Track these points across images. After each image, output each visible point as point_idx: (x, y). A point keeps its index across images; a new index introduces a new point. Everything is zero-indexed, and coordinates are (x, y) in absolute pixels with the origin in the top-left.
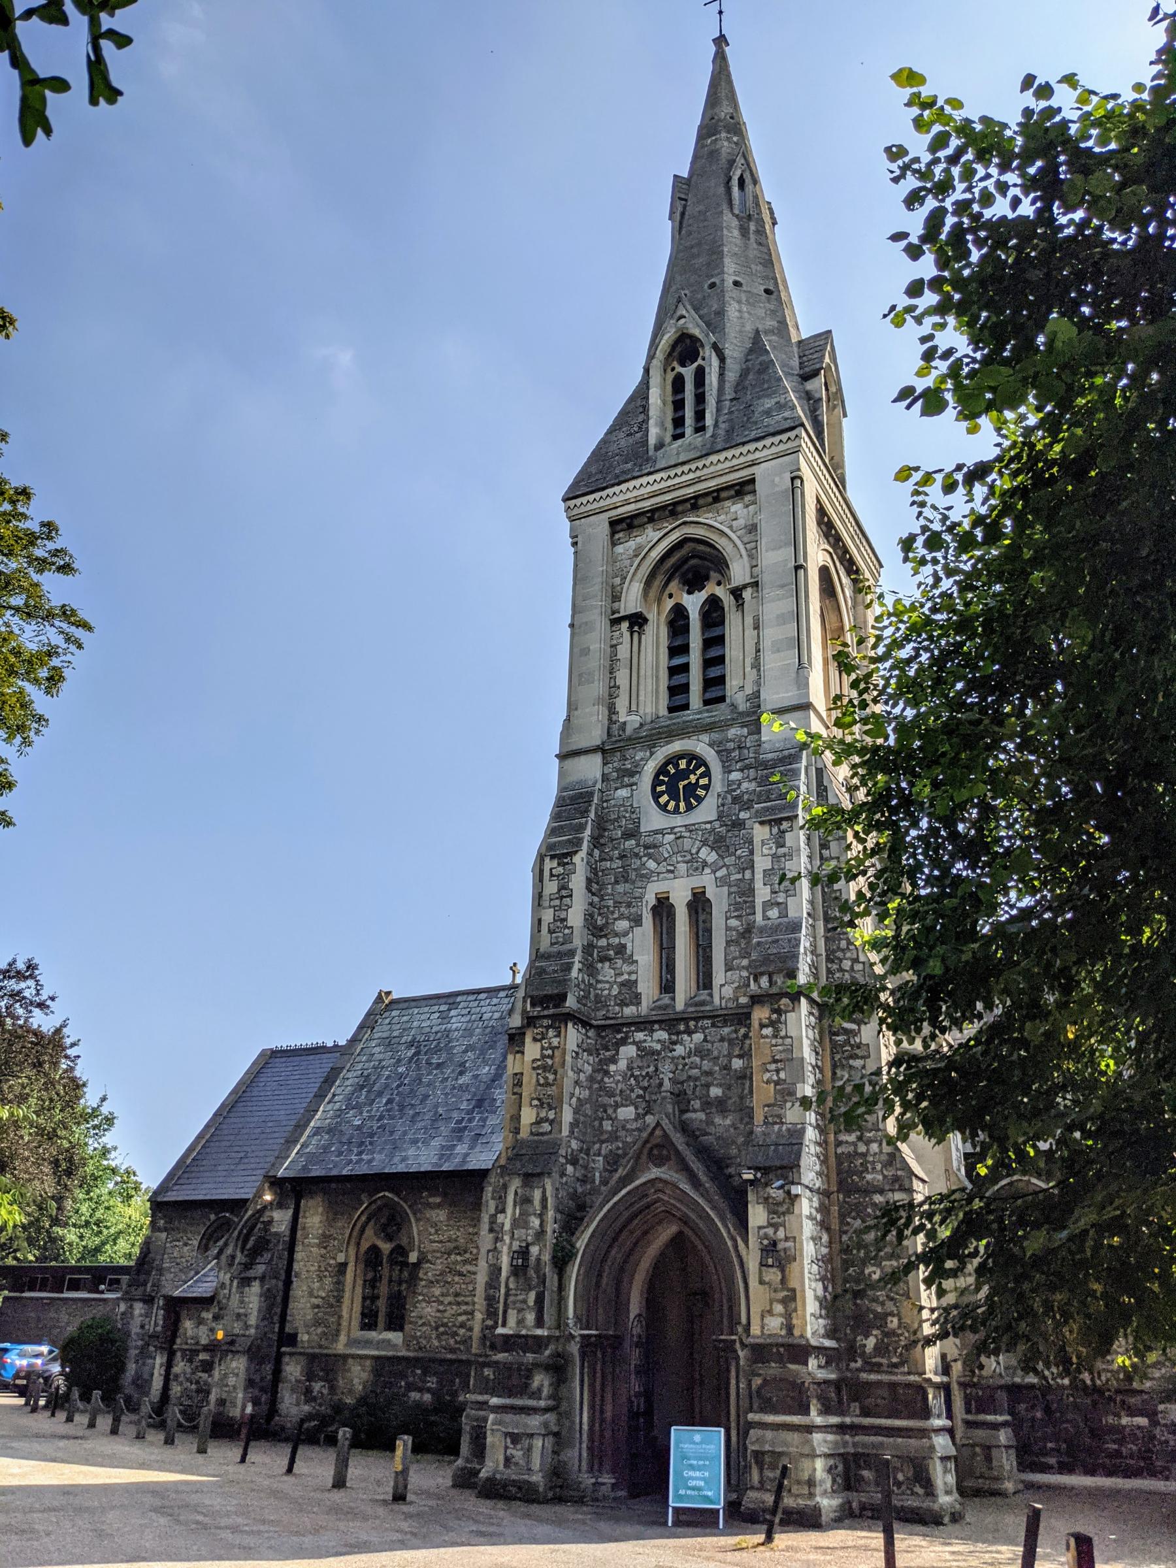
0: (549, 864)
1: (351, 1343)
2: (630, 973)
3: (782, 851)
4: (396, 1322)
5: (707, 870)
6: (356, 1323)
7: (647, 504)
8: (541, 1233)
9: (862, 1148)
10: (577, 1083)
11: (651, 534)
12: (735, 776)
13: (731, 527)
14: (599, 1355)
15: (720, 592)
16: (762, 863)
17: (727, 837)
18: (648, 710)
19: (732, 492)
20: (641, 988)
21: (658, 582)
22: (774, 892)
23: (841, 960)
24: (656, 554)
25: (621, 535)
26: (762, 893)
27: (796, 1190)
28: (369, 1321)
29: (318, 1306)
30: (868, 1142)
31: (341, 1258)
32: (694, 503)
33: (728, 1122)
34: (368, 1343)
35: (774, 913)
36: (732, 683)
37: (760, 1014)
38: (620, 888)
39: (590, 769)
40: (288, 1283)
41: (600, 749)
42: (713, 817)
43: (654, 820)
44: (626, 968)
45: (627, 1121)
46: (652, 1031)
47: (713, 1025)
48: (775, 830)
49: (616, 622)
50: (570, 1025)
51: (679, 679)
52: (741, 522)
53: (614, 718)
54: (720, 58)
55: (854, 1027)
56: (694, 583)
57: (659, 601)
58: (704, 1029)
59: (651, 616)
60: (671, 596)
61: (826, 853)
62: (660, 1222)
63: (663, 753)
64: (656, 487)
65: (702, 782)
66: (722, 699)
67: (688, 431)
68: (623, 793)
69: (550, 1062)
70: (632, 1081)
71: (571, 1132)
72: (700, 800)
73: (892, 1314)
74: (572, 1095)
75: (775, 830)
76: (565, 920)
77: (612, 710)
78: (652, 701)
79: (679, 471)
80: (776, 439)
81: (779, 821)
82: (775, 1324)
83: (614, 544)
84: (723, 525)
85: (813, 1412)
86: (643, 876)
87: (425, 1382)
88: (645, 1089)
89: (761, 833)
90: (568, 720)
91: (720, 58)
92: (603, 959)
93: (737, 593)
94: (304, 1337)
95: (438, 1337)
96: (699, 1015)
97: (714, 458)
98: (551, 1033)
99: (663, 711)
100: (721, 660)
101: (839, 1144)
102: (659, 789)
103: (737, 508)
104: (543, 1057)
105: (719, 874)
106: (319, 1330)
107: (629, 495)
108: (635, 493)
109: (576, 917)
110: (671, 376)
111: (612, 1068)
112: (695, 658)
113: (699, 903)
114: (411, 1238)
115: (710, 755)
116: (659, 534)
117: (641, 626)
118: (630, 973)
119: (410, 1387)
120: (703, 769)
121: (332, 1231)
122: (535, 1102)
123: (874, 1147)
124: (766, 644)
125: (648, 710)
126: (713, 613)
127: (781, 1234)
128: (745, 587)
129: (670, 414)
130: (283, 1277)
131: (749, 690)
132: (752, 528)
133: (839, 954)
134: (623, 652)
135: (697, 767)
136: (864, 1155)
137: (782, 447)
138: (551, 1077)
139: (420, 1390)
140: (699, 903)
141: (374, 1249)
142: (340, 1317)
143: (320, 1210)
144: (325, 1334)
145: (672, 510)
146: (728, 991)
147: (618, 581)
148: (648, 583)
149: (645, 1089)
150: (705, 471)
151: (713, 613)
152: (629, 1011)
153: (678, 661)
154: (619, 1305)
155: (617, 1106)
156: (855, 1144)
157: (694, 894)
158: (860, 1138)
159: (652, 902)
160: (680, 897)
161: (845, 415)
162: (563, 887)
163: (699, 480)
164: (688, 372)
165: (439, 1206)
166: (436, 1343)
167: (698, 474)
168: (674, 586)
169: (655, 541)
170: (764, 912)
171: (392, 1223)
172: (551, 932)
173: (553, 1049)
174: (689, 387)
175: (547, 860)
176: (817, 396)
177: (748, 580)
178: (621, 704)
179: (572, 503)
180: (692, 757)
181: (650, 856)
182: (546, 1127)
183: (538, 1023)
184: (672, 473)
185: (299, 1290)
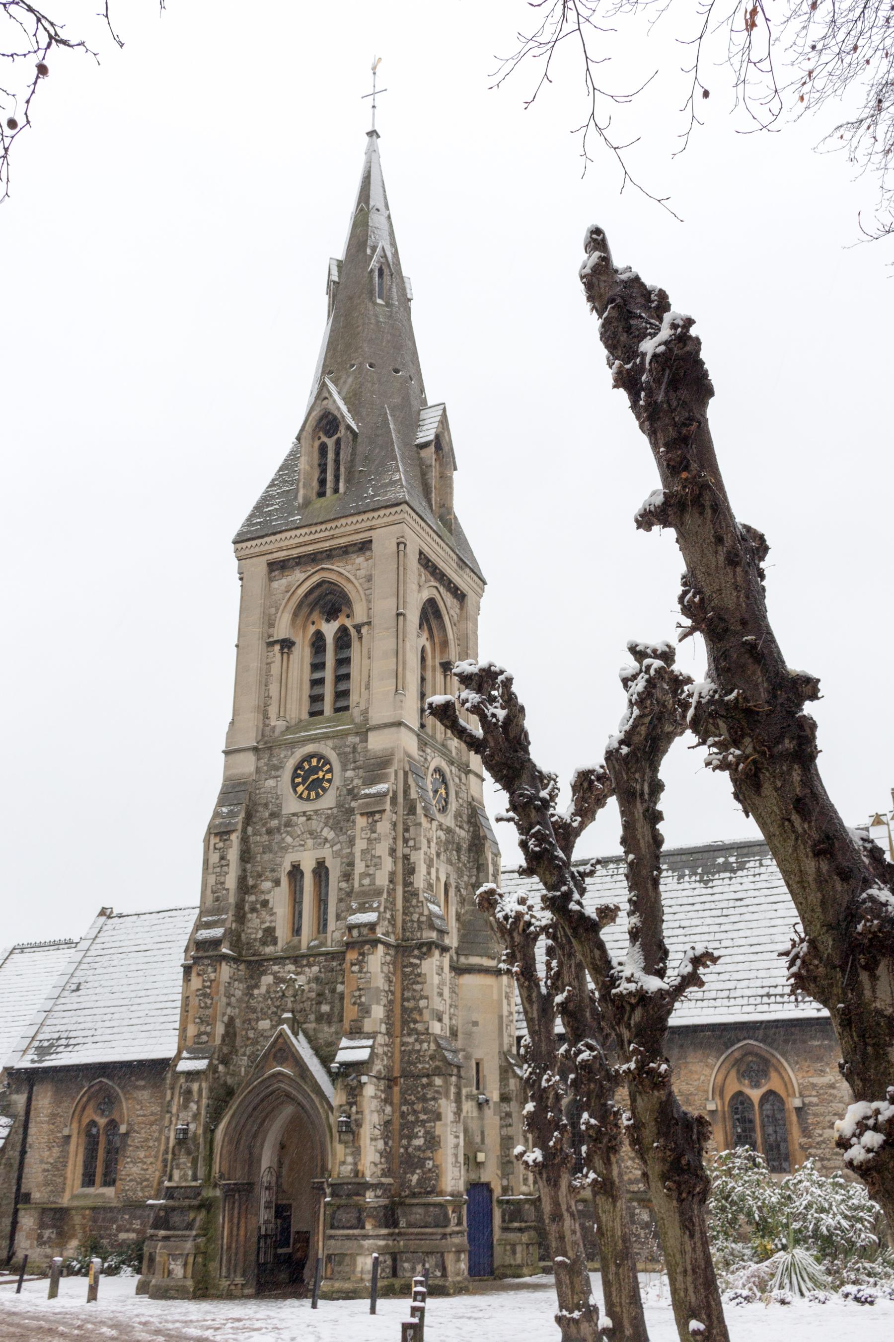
0: (213, 840)
1: (74, 1197)
2: (271, 922)
3: (374, 835)
4: (109, 1181)
5: (327, 845)
6: (78, 1182)
7: (295, 552)
8: (196, 1116)
9: (417, 1047)
10: (228, 1004)
11: (298, 575)
12: (350, 774)
13: (355, 575)
14: (237, 1197)
15: (348, 623)
16: (361, 844)
17: (341, 819)
18: (293, 716)
19: (356, 548)
20: (279, 933)
21: (299, 621)
22: (367, 866)
23: (412, 914)
24: (302, 591)
25: (276, 573)
26: (360, 867)
27: (364, 1079)
28: (89, 1179)
29: (48, 1170)
30: (421, 1042)
31: (66, 1132)
32: (330, 555)
33: (333, 1030)
34: (85, 1196)
35: (366, 881)
36: (354, 698)
37: (351, 956)
38: (267, 857)
39: (247, 764)
40: (23, 1153)
41: (255, 749)
42: (333, 805)
43: (292, 805)
44: (268, 918)
45: (265, 1030)
46: (285, 965)
47: (326, 960)
48: (370, 820)
49: (271, 644)
50: (224, 964)
51: (317, 691)
52: (362, 573)
53: (267, 722)
54: (372, 153)
55: (418, 962)
56: (332, 613)
57: (305, 628)
58: (319, 963)
59: (298, 640)
60: (313, 623)
61: (407, 835)
62: (282, 1103)
63: (301, 752)
64: (302, 539)
65: (328, 776)
66: (347, 708)
67: (329, 491)
68: (271, 783)
69: (208, 991)
70: (269, 1002)
71: (223, 1040)
72: (325, 790)
73: (430, 1159)
74: (224, 1014)
75: (370, 820)
76: (223, 883)
77: (266, 717)
78: (297, 707)
79: (318, 528)
80: (387, 511)
81: (372, 814)
82: (346, 1170)
83: (271, 580)
84: (347, 573)
85: (368, 1226)
86: (283, 848)
87: (132, 1224)
88: (277, 1007)
89: (361, 822)
90: (232, 723)
91: (372, 153)
92: (253, 910)
93: (358, 628)
94: (36, 1196)
95: (142, 1190)
96: (313, 955)
97: (343, 521)
98: (210, 969)
99: (305, 716)
100: (347, 677)
101: (403, 1044)
102: (297, 780)
103: (360, 560)
104: (204, 987)
105: (335, 848)
106: (50, 1188)
107: (282, 544)
108: (287, 543)
109: (231, 882)
110: (317, 444)
111: (256, 992)
112: (329, 674)
113: (321, 870)
114: (122, 1114)
115: (333, 756)
116: (303, 576)
117: (289, 648)
118: (271, 922)
119: (120, 1229)
120: (328, 766)
121: (60, 1110)
122: (197, 1020)
123: (425, 1045)
124: (375, 673)
125: (293, 716)
126: (343, 639)
127: (354, 1109)
128: (363, 624)
129: (316, 475)
130: (19, 1149)
131: (363, 707)
132: (369, 579)
133: (411, 909)
134: (275, 669)
135: (324, 765)
136: (419, 1051)
137: (392, 518)
138: (209, 1002)
139: (128, 1231)
140: (321, 870)
141: (93, 1123)
142: (65, 1178)
143: (49, 1094)
144: (52, 1191)
145: (313, 558)
146: (337, 935)
147: (273, 610)
148: (295, 615)
149: (277, 1007)
150: (337, 531)
151: (343, 639)
152: (269, 950)
153: (317, 675)
154: (252, 1162)
155: (258, 1020)
156: (413, 1044)
157: (318, 863)
158: (416, 1040)
159: (288, 868)
160: (308, 867)
161: (455, 469)
162: (222, 858)
163: (333, 537)
164: (330, 443)
165: (144, 1088)
166: (140, 1194)
167: (332, 532)
168: (315, 616)
169: (300, 581)
170: (360, 880)
171: (107, 1101)
172: (213, 892)
173: (211, 981)
174: (331, 455)
175: (212, 836)
176: (428, 462)
177: (365, 620)
178: (273, 711)
179: (239, 546)
180: (320, 757)
181: (288, 833)
182: (204, 1038)
183: (201, 962)
184: (313, 529)
185: (32, 1157)
